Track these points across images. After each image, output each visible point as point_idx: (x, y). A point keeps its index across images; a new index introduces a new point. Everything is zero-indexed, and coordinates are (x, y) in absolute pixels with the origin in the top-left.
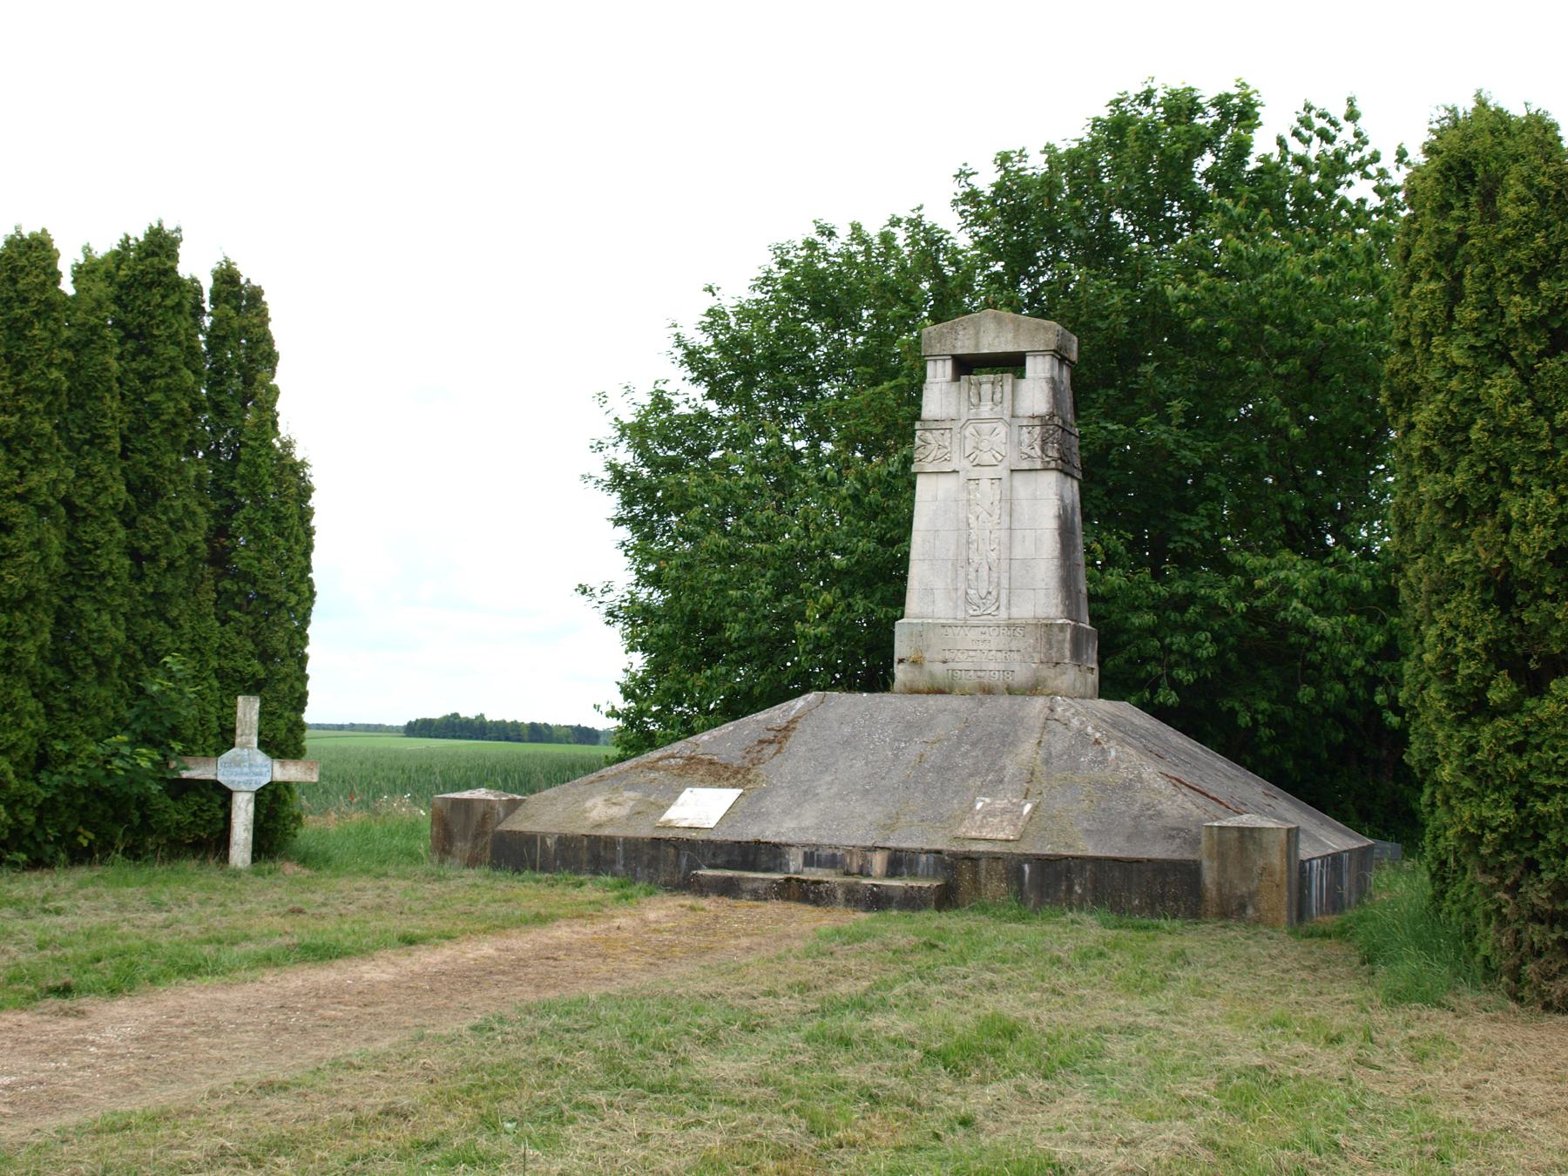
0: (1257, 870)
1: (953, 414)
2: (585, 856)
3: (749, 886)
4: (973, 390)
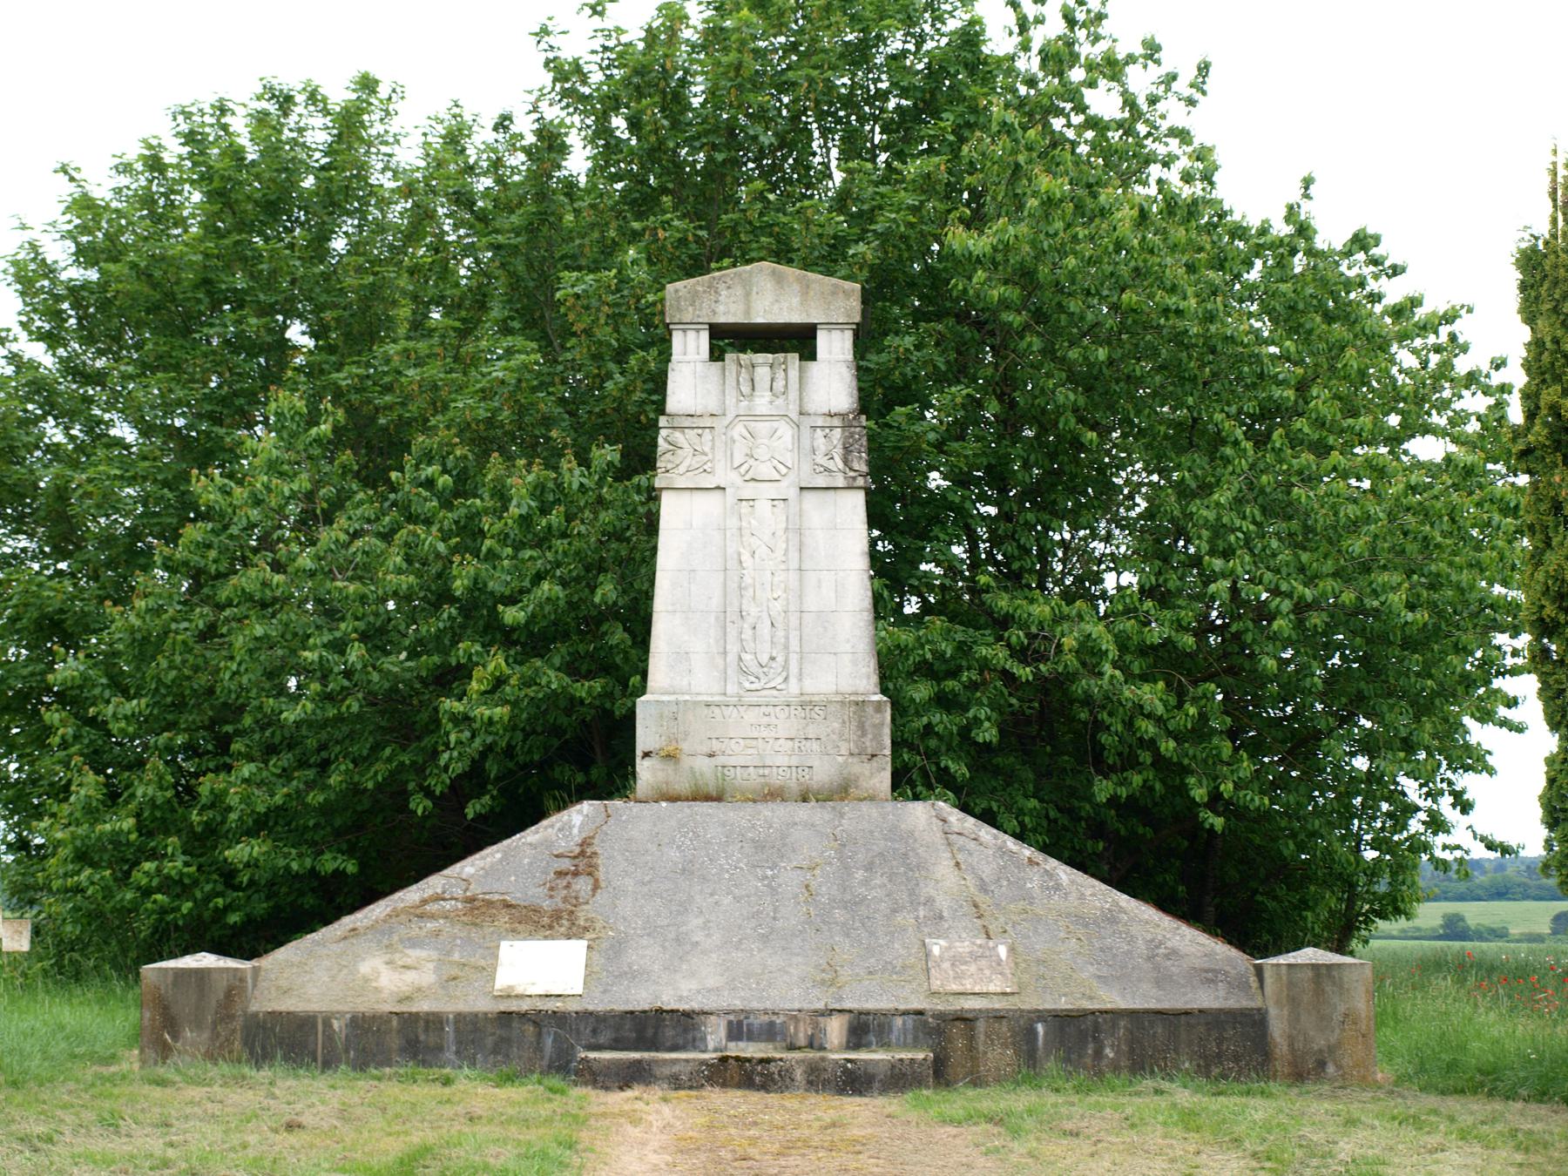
0: (1337, 1017)
1: (713, 406)
2: (395, 1042)
3: (666, 1071)
4: (744, 375)
